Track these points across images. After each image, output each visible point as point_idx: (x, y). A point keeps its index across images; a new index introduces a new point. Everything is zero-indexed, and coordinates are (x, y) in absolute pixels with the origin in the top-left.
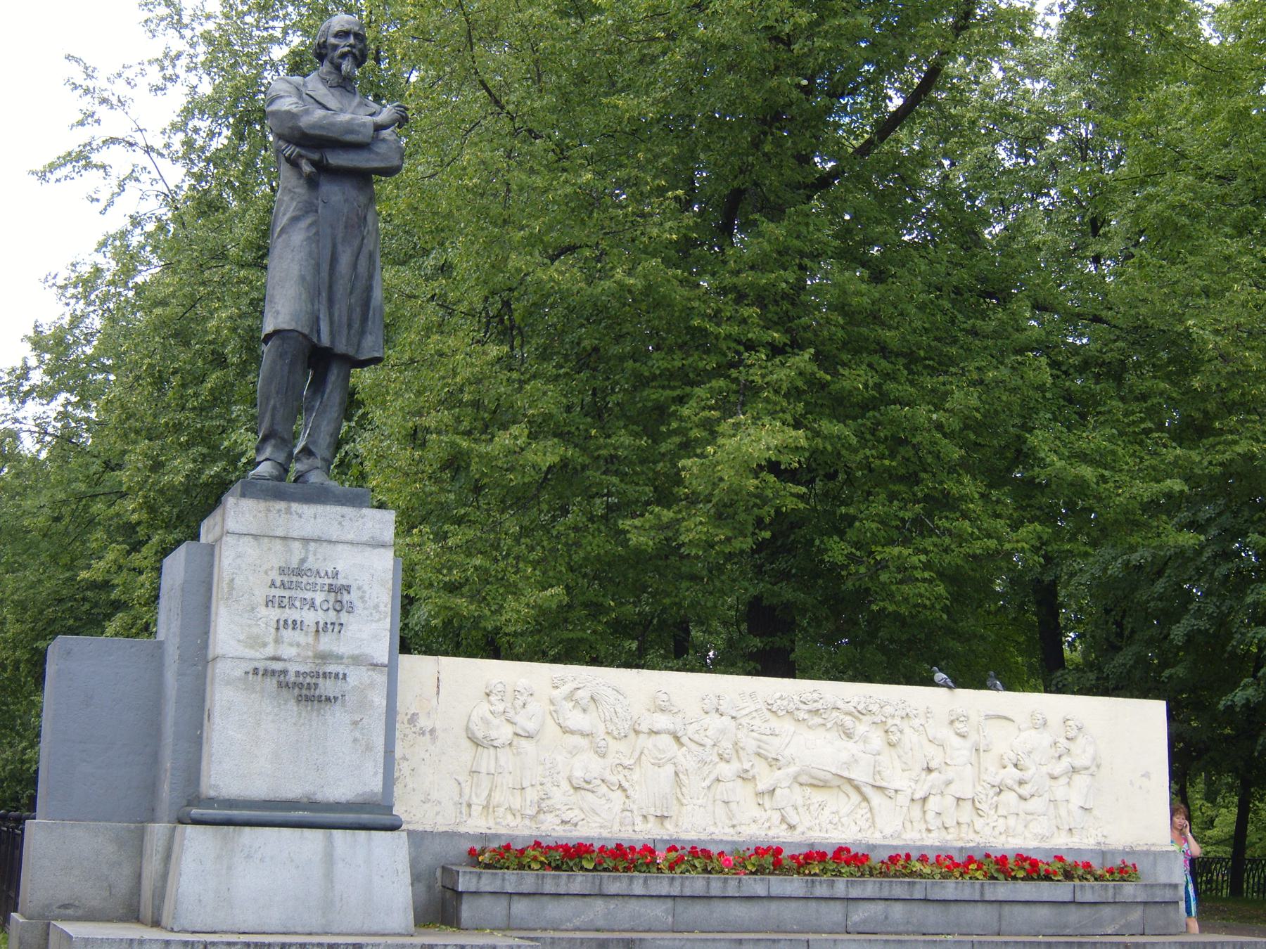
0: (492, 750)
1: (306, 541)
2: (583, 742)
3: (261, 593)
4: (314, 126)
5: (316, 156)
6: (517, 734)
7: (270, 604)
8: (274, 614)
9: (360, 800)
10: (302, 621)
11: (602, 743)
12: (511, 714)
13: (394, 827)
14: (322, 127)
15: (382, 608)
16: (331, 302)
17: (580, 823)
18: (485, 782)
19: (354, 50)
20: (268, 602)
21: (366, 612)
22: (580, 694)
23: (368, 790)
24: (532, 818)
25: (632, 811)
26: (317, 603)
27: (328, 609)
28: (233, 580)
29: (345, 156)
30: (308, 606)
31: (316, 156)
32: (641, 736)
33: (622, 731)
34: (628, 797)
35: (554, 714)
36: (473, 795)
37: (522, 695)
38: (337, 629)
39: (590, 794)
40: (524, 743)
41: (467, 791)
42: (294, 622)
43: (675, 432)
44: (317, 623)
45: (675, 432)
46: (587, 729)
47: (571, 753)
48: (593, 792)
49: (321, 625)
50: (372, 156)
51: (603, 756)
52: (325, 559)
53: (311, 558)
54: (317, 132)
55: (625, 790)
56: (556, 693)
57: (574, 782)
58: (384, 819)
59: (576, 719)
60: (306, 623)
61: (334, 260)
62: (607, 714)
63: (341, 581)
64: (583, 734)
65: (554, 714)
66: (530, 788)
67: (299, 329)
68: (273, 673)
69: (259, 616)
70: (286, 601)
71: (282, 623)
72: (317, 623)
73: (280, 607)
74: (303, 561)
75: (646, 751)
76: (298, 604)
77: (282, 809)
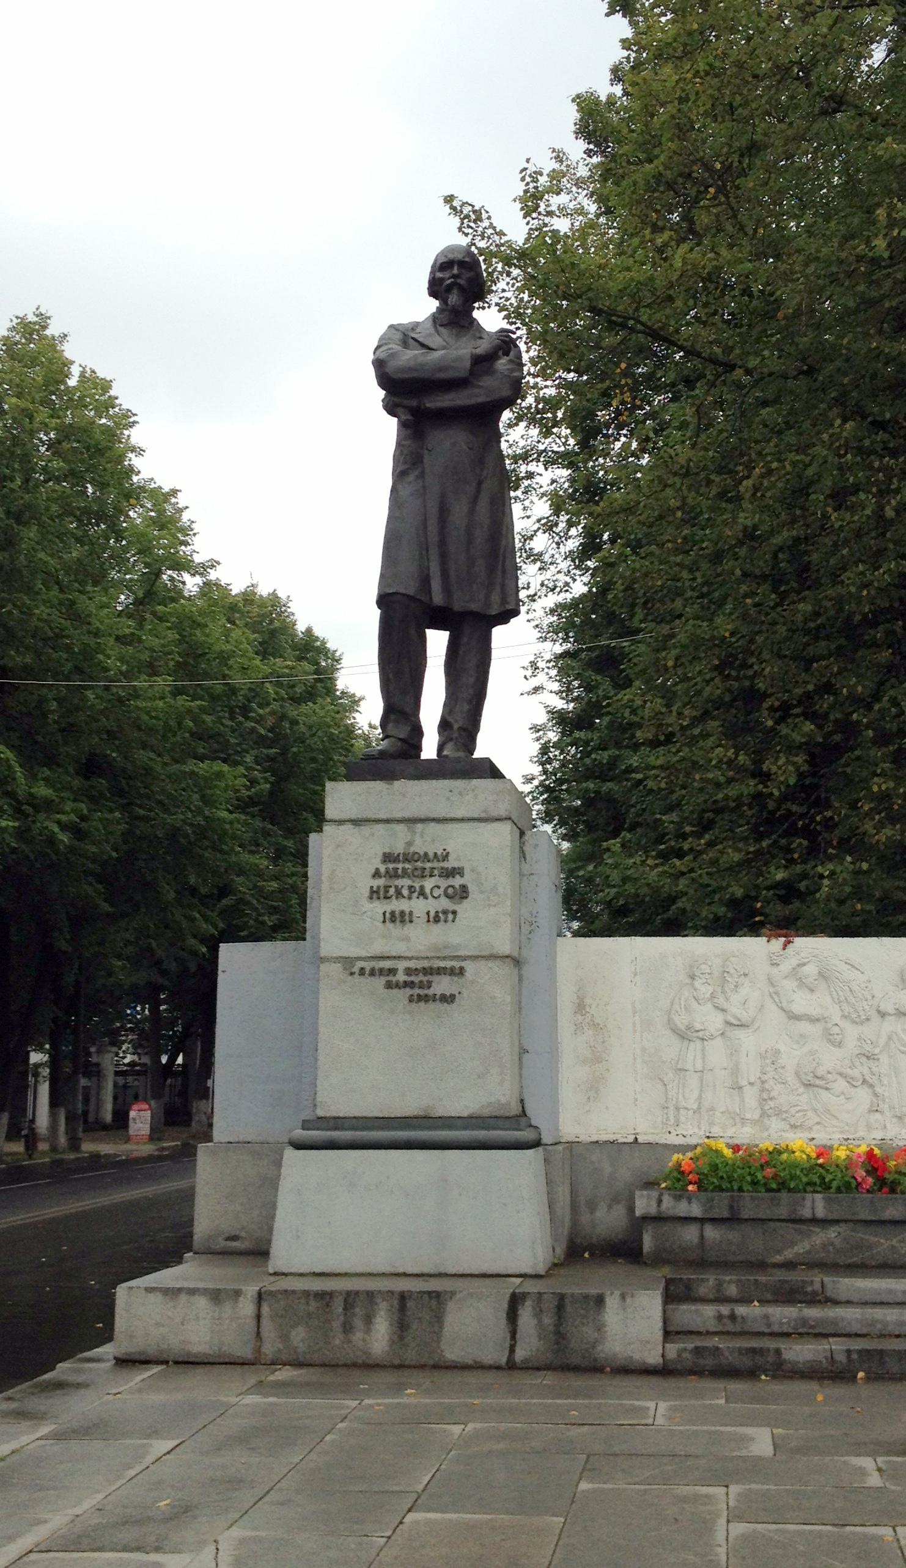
0: (699, 1043)
1: (412, 821)
2: (815, 1030)
3: (367, 883)
4: (402, 370)
5: (414, 403)
6: (728, 1023)
7: (375, 896)
8: (380, 907)
9: (486, 1112)
10: (411, 913)
11: (836, 1030)
12: (721, 1001)
13: (536, 1144)
14: (411, 369)
15: (501, 889)
16: (444, 557)
17: (815, 1128)
18: (693, 1082)
19: (459, 281)
20: (374, 894)
21: (482, 896)
22: (806, 969)
23: (493, 1100)
24: (754, 1123)
25: (882, 1113)
26: (428, 891)
27: (439, 896)
28: (333, 871)
29: (447, 397)
30: (416, 894)
31: (414, 403)
32: (888, 1018)
33: (862, 1013)
34: (876, 1095)
35: (775, 994)
36: (680, 1096)
37: (731, 976)
38: (450, 917)
39: (823, 1093)
40: (740, 1033)
41: (672, 1093)
42: (402, 913)
43: (731, 614)
44: (428, 913)
45: (731, 614)
46: (814, 1012)
47: (798, 1042)
48: (827, 1089)
49: (432, 914)
50: (476, 391)
51: (839, 1045)
52: (433, 841)
53: (418, 841)
54: (406, 376)
55: (872, 1086)
56: (775, 971)
57: (803, 1077)
58: (526, 1135)
59: (801, 1002)
60: (416, 914)
61: (444, 511)
62: (841, 993)
63: (450, 864)
64: (814, 1020)
65: (775, 994)
66: (748, 1087)
67: (403, 591)
68: (381, 970)
69: (364, 910)
70: (392, 891)
71: (388, 915)
72: (428, 913)
73: (386, 898)
74: (409, 844)
75: (895, 1038)
76: (405, 892)
77: (402, 1128)
